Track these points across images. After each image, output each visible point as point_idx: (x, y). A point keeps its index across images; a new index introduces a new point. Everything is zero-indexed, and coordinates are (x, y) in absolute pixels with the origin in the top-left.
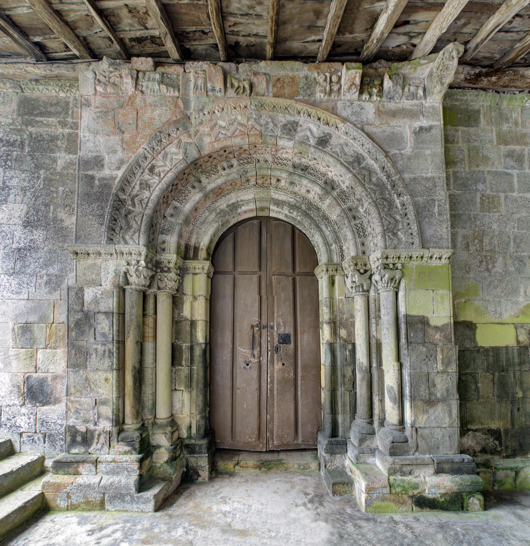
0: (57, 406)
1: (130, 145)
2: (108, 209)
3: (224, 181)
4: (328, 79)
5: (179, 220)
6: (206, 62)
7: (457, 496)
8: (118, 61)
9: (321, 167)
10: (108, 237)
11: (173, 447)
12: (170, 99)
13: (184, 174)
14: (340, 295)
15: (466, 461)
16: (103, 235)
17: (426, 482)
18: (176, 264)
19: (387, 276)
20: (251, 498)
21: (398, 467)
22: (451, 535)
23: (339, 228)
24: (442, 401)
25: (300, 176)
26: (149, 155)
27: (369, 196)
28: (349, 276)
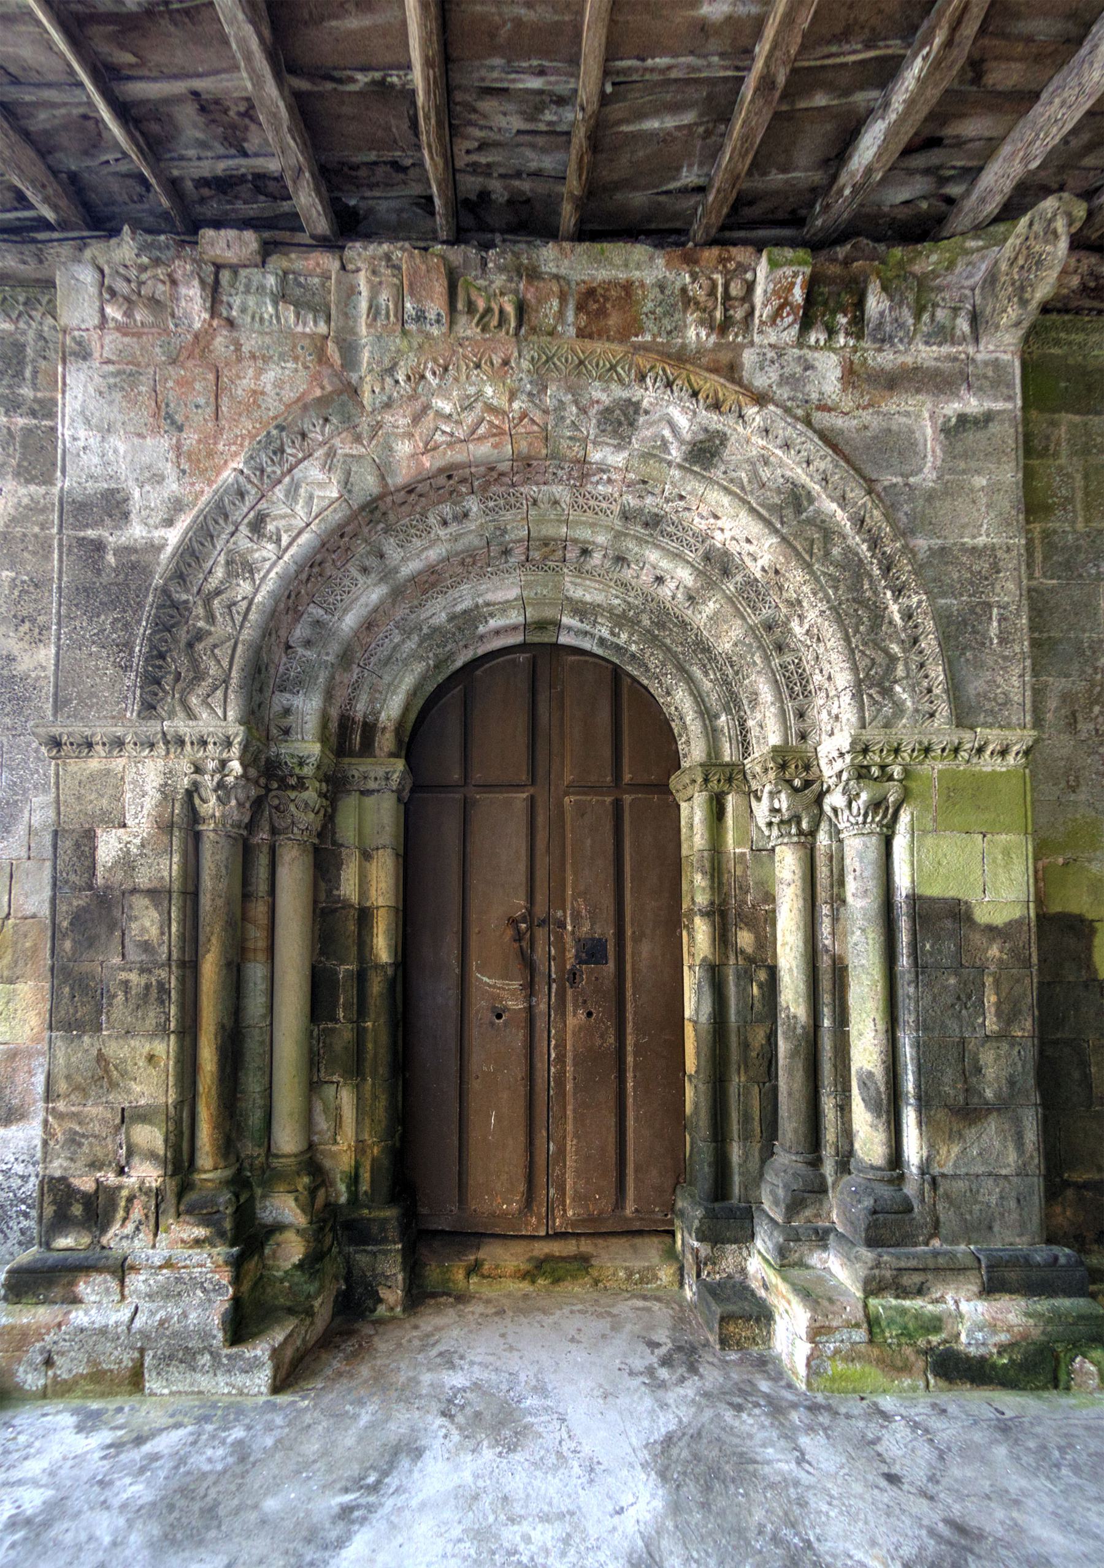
0: (14, 1128)
1: (199, 461)
2: (143, 629)
3: (444, 554)
4: (720, 289)
5: (327, 654)
6: (399, 244)
7: (1042, 1352)
8: (162, 238)
9: (697, 520)
10: (143, 701)
11: (314, 1226)
12: (306, 342)
13: (342, 536)
14: (738, 844)
15: (1062, 1260)
16: (130, 695)
17: (961, 1316)
18: (318, 767)
19: (864, 796)
20: (516, 1354)
21: (888, 1274)
22: (1029, 1449)
23: (737, 673)
24: (998, 1110)
25: (640, 541)
26: (249, 487)
27: (820, 595)
28: (765, 797)
